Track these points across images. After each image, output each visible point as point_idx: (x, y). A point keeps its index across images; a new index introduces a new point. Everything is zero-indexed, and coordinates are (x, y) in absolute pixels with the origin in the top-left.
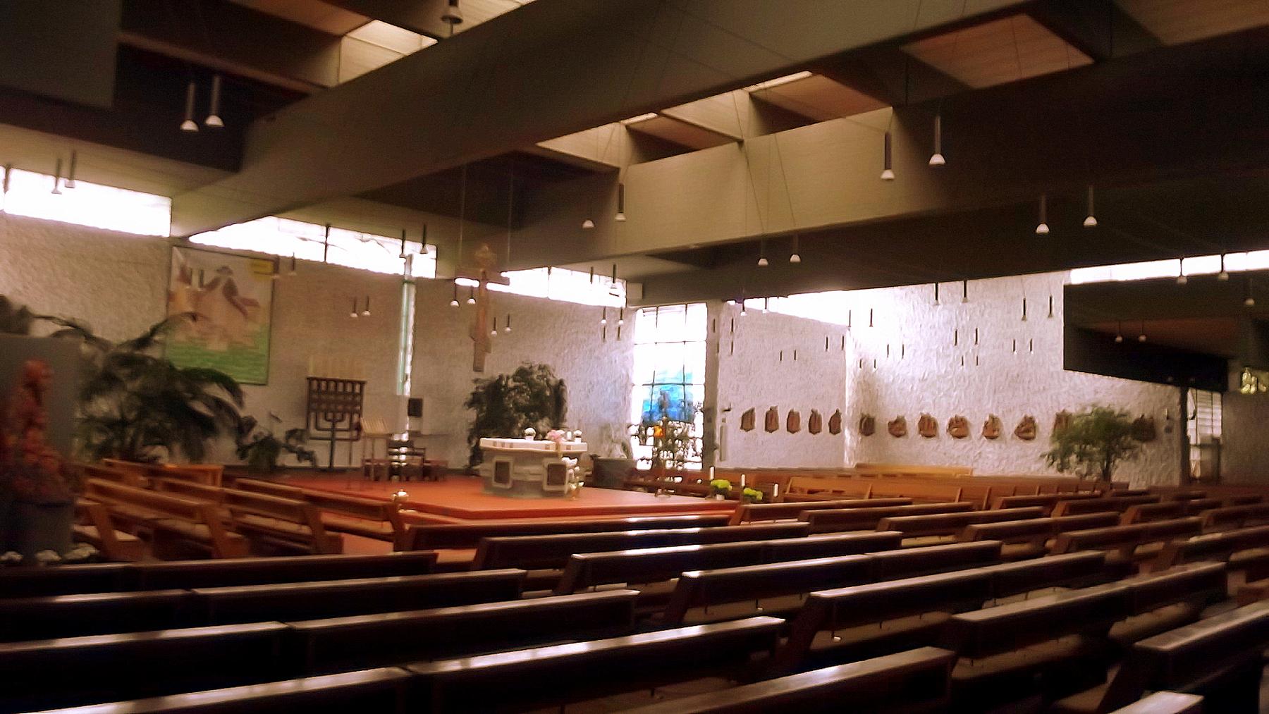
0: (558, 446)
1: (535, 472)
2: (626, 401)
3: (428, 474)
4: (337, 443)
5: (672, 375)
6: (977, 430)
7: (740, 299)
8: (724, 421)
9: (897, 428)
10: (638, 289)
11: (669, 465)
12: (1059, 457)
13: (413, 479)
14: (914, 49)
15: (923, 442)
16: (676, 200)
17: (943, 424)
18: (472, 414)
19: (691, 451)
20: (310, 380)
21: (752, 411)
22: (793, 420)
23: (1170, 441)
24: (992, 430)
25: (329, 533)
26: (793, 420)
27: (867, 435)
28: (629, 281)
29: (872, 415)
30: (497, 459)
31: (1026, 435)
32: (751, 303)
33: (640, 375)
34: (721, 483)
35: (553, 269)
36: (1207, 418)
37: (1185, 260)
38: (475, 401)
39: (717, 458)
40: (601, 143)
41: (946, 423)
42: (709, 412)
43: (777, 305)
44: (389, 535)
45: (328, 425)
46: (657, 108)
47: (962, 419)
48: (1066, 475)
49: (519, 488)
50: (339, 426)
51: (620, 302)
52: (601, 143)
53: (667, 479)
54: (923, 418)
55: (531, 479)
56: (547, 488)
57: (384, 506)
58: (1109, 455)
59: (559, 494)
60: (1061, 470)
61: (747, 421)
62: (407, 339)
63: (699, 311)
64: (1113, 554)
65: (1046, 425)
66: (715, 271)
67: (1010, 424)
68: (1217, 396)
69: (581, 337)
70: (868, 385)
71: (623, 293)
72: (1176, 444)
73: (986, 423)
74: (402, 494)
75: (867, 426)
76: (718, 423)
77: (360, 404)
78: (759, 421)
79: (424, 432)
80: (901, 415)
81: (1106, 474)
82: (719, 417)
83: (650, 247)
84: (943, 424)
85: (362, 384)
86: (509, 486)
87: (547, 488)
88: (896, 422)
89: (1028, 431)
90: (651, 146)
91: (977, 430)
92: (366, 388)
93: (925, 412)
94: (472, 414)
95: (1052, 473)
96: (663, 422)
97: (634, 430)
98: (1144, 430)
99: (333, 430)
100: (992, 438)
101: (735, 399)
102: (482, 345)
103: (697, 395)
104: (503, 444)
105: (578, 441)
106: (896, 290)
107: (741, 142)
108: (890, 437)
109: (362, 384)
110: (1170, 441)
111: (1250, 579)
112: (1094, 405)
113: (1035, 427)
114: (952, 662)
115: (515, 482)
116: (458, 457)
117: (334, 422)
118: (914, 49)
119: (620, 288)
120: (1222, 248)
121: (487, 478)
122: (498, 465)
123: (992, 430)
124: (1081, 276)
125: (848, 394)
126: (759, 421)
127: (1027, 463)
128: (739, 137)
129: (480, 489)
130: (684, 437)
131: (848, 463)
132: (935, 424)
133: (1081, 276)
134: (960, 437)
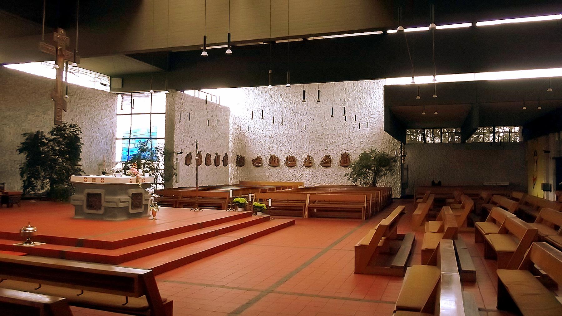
0: (137, 179)
1: (124, 199)
2: (113, 149)
6: (300, 162)
8: (177, 160)
9: (257, 162)
10: (118, 83)
17: (283, 159)
18: (22, 158)
21: (191, 153)
24: (309, 163)
27: (241, 166)
28: (112, 77)
30: (88, 191)
31: (326, 165)
39: (174, 181)
42: (169, 154)
49: (112, 212)
51: (107, 89)
55: (122, 205)
58: (377, 174)
63: (160, 99)
65: (336, 160)
67: (318, 160)
69: (87, 109)
70: (241, 140)
73: (306, 159)
75: (241, 162)
80: (259, 155)
81: (375, 182)
84: (283, 159)
86: (101, 212)
87: (131, 211)
88: (256, 159)
89: (327, 163)
91: (300, 162)
93: (272, 154)
95: (350, 183)
101: (183, 146)
103: (160, 144)
105: (147, 175)
106: (243, 89)
108: (253, 167)
113: (331, 161)
115: (106, 209)
119: (106, 80)
121: (82, 206)
122: (89, 195)
123: (309, 163)
125: (230, 144)
127: (338, 177)
131: (231, 181)
133: (392, 81)
134: (291, 167)
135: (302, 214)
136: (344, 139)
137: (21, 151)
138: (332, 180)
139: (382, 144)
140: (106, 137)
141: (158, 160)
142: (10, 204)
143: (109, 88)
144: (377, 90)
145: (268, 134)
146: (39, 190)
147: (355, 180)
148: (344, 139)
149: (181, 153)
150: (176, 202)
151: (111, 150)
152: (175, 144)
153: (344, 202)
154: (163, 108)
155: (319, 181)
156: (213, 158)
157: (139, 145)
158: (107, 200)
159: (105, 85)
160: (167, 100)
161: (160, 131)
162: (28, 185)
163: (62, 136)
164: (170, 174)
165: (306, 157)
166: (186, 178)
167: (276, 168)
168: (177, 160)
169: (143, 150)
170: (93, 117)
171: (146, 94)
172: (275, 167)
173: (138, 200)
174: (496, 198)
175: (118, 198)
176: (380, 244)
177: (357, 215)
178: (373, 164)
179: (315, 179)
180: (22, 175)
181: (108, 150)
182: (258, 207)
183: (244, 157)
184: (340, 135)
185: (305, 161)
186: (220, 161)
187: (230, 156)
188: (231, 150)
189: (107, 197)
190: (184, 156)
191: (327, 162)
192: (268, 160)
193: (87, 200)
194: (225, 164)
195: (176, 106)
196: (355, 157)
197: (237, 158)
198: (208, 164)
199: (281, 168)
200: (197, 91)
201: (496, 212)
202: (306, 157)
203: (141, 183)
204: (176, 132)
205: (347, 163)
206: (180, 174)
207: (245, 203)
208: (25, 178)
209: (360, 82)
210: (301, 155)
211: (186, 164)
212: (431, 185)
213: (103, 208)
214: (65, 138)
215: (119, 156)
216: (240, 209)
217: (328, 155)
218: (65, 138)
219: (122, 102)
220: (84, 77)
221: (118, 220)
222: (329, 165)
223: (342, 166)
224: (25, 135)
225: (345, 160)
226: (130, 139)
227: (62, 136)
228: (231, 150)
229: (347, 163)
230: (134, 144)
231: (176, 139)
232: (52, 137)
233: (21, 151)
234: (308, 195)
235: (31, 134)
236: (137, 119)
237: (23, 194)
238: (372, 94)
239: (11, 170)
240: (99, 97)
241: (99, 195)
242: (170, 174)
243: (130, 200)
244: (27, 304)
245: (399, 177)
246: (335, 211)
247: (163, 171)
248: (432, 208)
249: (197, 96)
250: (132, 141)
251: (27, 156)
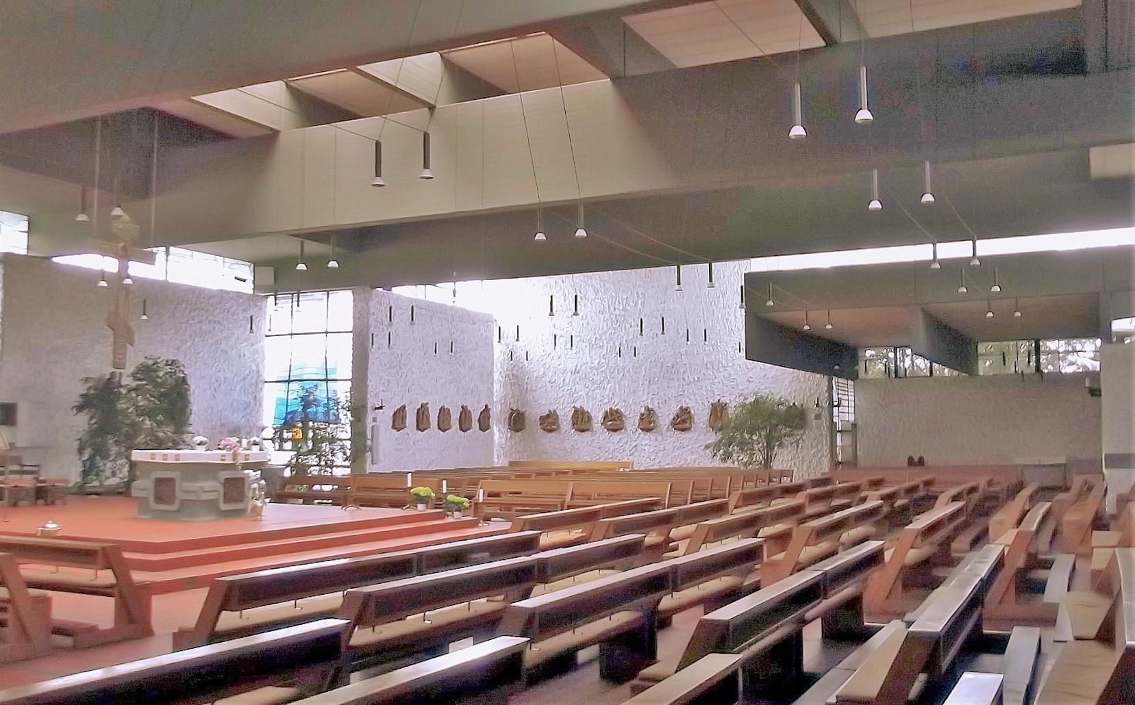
0: (235, 456)
1: (210, 488)
2: (257, 399)
3: (43, 495)
5: (313, 370)
6: (632, 422)
7: (388, 287)
8: (374, 420)
9: (549, 422)
10: (268, 274)
11: (314, 471)
12: (724, 447)
13: (21, 503)
14: (629, 20)
15: (578, 437)
16: (334, 175)
17: (598, 417)
18: (82, 422)
19: (340, 455)
22: (422, 413)
23: (819, 428)
24: (648, 422)
25: (34, 592)
26: (422, 413)
27: (517, 431)
29: (522, 410)
32: (396, 290)
33: (273, 369)
34: (423, 491)
35: (172, 248)
36: (848, 404)
38: (85, 404)
39: (369, 461)
40: (260, 102)
41: (601, 416)
42: (358, 409)
43: (439, 294)
44: (112, 587)
46: (351, 63)
47: (617, 411)
48: (729, 464)
49: (190, 508)
51: (248, 288)
52: (260, 102)
53: (317, 487)
55: (205, 496)
56: (223, 507)
57: (103, 549)
59: (240, 513)
60: (724, 460)
61: (398, 420)
63: (343, 300)
64: (652, 538)
65: (701, 414)
66: (364, 254)
67: (665, 416)
68: (851, 383)
70: (517, 379)
71: (250, 277)
72: (825, 431)
74: (51, 526)
75: (517, 421)
76: (369, 423)
78: (411, 419)
79: (19, 445)
81: (767, 462)
82: (370, 415)
83: (294, 226)
84: (598, 417)
86: (174, 507)
87: (223, 507)
88: (548, 416)
89: (684, 421)
90: (318, 110)
91: (632, 422)
93: (578, 405)
94: (82, 422)
95: (717, 463)
96: (300, 420)
97: (269, 433)
98: (795, 418)
100: (648, 430)
101: (386, 393)
102: (123, 336)
103: (342, 391)
107: (432, 108)
108: (541, 431)
110: (819, 428)
111: (641, 541)
112: (755, 394)
114: (349, 629)
115: (183, 502)
116: (66, 469)
118: (629, 20)
119: (246, 271)
120: (972, 236)
121: (146, 499)
122: (159, 481)
123: (648, 422)
124: (760, 265)
125: (496, 387)
126: (411, 419)
127: (693, 452)
128: (432, 102)
129: (133, 510)
130: (333, 440)
131: (499, 460)
132: (589, 418)
133: (760, 265)
134: (615, 430)
137: (80, 408)
138: (693, 457)
139: (791, 382)
140: (244, 379)
141: (337, 421)
142: (49, 500)
145: (570, 365)
146: (107, 478)
147: (727, 456)
149: (381, 408)
150: (345, 497)
151: (254, 404)
152: (370, 389)
155: (669, 460)
156: (455, 417)
157: (302, 393)
158: (184, 488)
160: (355, 306)
161: (343, 367)
162: (89, 470)
163: (152, 381)
164: (360, 448)
165: (643, 410)
166: (395, 453)
168: (374, 420)
169: (307, 402)
171: (318, 295)
172: (583, 431)
173: (235, 488)
179: (660, 454)
180: (80, 451)
181: (247, 405)
182: (453, 503)
183: (523, 414)
185: (641, 419)
187: (495, 411)
188: (498, 396)
189: (184, 484)
190: (388, 413)
194: (484, 425)
195: (372, 318)
197: (511, 415)
198: (443, 426)
199: (594, 433)
202: (643, 410)
203: (241, 460)
204: (373, 367)
206: (381, 448)
207: (429, 497)
208: (85, 457)
211: (393, 427)
212: (906, 464)
213: (177, 502)
214: (157, 385)
215: (269, 417)
216: (421, 507)
217: (685, 406)
218: (157, 385)
219: (277, 313)
224: (87, 380)
227: (152, 381)
231: (372, 382)
233: (80, 408)
235: (100, 379)
237: (82, 486)
240: (228, 305)
241: (172, 480)
242: (360, 448)
243: (221, 490)
247: (348, 444)
249: (421, 297)
250: (294, 386)
251: (92, 418)
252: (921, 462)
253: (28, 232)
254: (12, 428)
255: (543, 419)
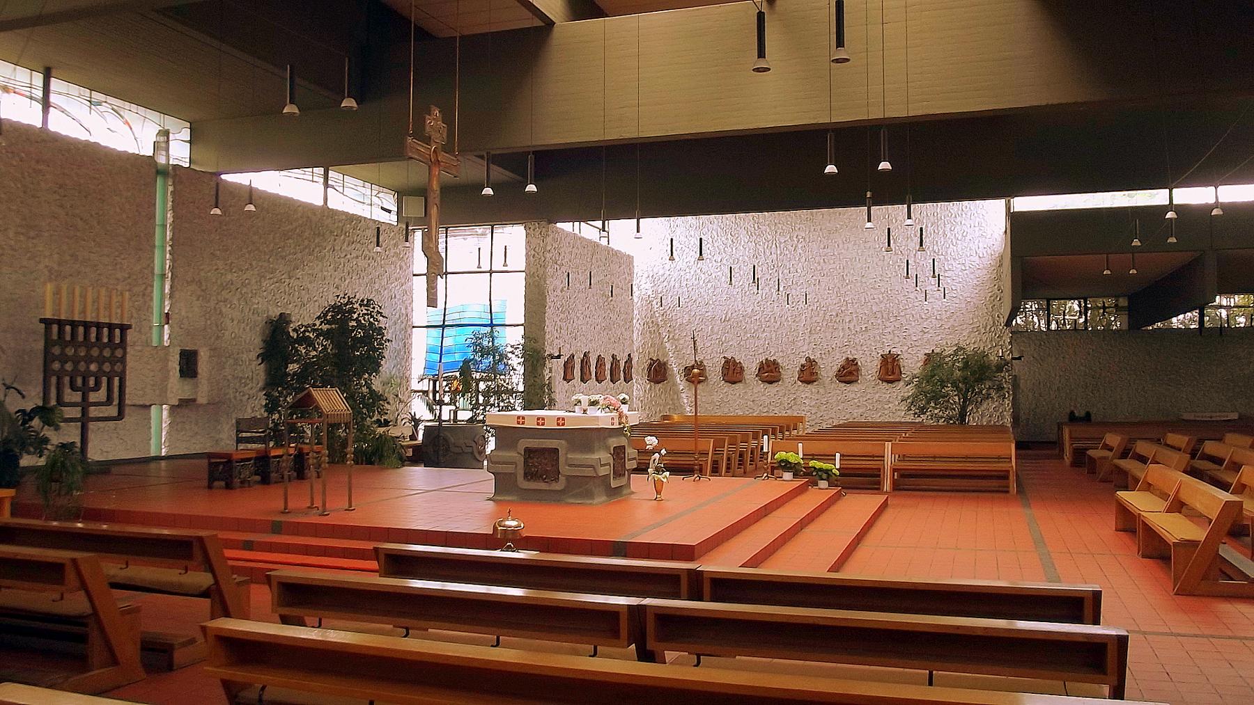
4: (92, 425)
6: (790, 371)
15: (727, 388)
17: (751, 368)
20: (47, 322)
28: (401, 194)
30: (525, 443)
31: (848, 378)
32: (559, 225)
37: (1220, 188)
42: (534, 357)
45: (77, 397)
49: (582, 487)
50: (93, 397)
51: (393, 218)
54: (727, 361)
62: (162, 259)
65: (870, 367)
67: (829, 367)
69: (362, 263)
75: (658, 372)
77: (123, 360)
81: (962, 415)
84: (751, 368)
85: (124, 328)
89: (851, 373)
92: (131, 336)
96: (470, 374)
99: (85, 405)
100: (809, 382)
103: (511, 338)
104: (540, 420)
109: (124, 328)
113: (858, 370)
115: (568, 478)
117: (85, 392)
119: (390, 201)
122: (529, 452)
123: (809, 374)
124: (1026, 204)
127: (889, 404)
133: (1026, 204)
134: (771, 383)
135: (879, 483)
136: (888, 324)
143: (395, 218)
144: (959, 219)
147: (922, 410)
148: (888, 324)
152: (547, 337)
153: (966, 458)
154: (518, 259)
158: (570, 460)
159: (389, 211)
160: (528, 243)
161: (513, 308)
167: (736, 386)
170: (373, 282)
171: (479, 230)
172: (734, 383)
174: (1142, 448)
175: (596, 456)
176: (229, 553)
177: (994, 484)
178: (956, 380)
182: (821, 470)
183: (665, 364)
184: (879, 315)
186: (619, 371)
191: (849, 373)
192: (719, 369)
193: (526, 462)
194: (628, 379)
196: (912, 364)
200: (577, 224)
201: (1154, 472)
205: (893, 373)
209: (955, 207)
210: (792, 357)
211: (565, 379)
217: (851, 357)
220: (358, 196)
221: (595, 501)
222: (853, 378)
223: (883, 380)
225: (890, 369)
226: (443, 326)
228: (637, 346)
229: (893, 373)
230: (454, 339)
232: (325, 327)
234: (888, 445)
236: (466, 290)
238: (948, 226)
239: (235, 398)
244: (1081, 639)
245: (1008, 402)
246: (991, 477)
248: (394, 458)
249: (577, 231)
252: (1087, 418)
253: (190, 142)
254: (191, 381)
255: (688, 371)
